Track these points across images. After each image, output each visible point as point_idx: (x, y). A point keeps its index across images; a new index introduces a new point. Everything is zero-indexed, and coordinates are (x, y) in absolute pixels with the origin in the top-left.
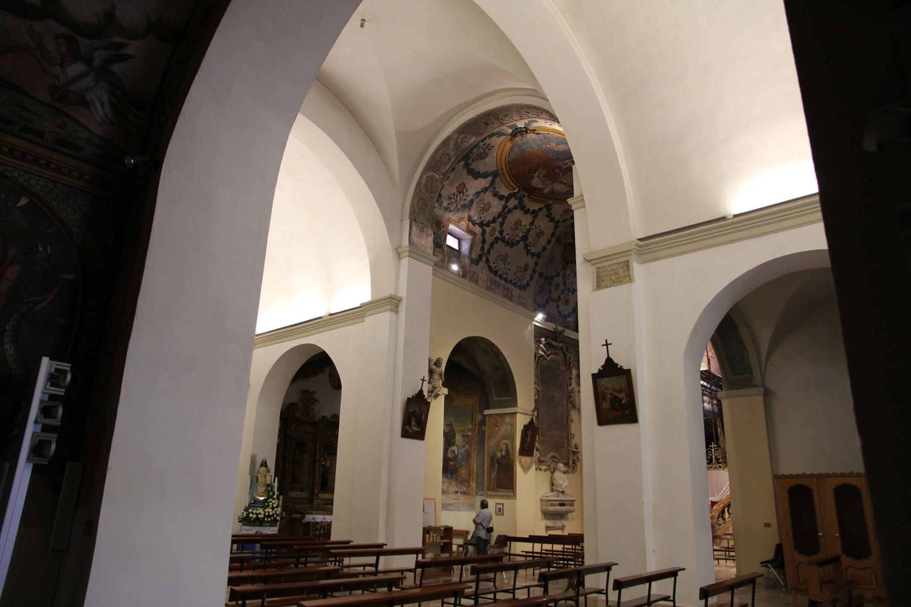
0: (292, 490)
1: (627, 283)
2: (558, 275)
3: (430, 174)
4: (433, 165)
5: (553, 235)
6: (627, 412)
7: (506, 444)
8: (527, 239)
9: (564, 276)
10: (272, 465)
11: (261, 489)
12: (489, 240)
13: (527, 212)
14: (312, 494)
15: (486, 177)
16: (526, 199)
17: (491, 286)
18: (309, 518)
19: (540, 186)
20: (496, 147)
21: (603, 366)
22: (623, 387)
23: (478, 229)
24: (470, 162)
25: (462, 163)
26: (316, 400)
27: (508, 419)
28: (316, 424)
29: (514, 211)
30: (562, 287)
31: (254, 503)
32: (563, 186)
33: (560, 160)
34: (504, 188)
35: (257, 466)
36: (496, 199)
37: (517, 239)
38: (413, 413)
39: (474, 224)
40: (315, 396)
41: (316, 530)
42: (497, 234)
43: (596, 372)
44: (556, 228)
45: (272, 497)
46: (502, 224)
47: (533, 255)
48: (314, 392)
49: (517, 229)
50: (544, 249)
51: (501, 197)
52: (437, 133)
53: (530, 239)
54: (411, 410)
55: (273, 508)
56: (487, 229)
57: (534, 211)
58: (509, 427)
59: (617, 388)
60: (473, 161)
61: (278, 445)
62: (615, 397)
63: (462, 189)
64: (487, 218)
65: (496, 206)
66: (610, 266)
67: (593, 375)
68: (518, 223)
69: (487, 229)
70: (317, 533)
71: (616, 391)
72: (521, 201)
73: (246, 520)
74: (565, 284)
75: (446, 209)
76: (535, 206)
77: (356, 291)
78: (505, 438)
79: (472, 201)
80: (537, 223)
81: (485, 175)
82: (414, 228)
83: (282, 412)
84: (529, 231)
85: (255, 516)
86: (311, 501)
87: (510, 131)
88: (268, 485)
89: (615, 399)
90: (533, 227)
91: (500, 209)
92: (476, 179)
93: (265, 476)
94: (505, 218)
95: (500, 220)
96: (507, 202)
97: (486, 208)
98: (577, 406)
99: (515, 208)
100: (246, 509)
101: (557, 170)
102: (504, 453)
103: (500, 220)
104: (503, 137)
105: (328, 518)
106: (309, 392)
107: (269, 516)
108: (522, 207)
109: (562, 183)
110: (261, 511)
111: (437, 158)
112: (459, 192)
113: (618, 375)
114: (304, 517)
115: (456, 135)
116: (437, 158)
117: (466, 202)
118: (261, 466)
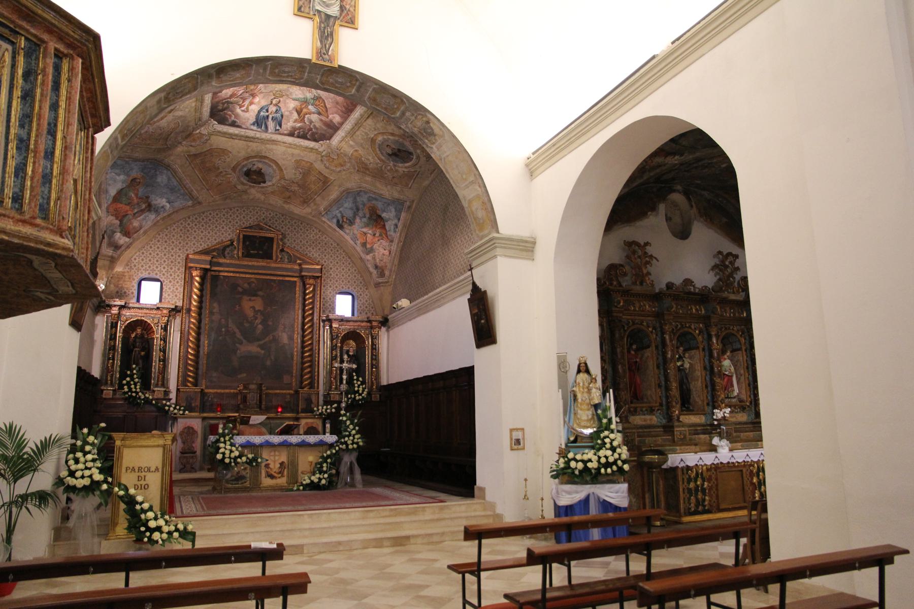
0: (634, 412)
10: (596, 368)
11: (585, 414)
14: (670, 418)
18: (675, 459)
26: (651, 256)
28: (657, 297)
31: (575, 441)
35: (569, 372)
40: (650, 250)
41: (689, 480)
45: (607, 428)
48: (647, 244)
55: (613, 449)
61: (602, 338)
70: (692, 485)
73: (565, 474)
83: (598, 280)
85: (580, 466)
86: (668, 428)
88: (596, 407)
93: (589, 391)
100: (563, 454)
105: (754, 455)
106: (638, 244)
107: (608, 465)
110: (590, 454)
114: (666, 461)
118: (579, 371)
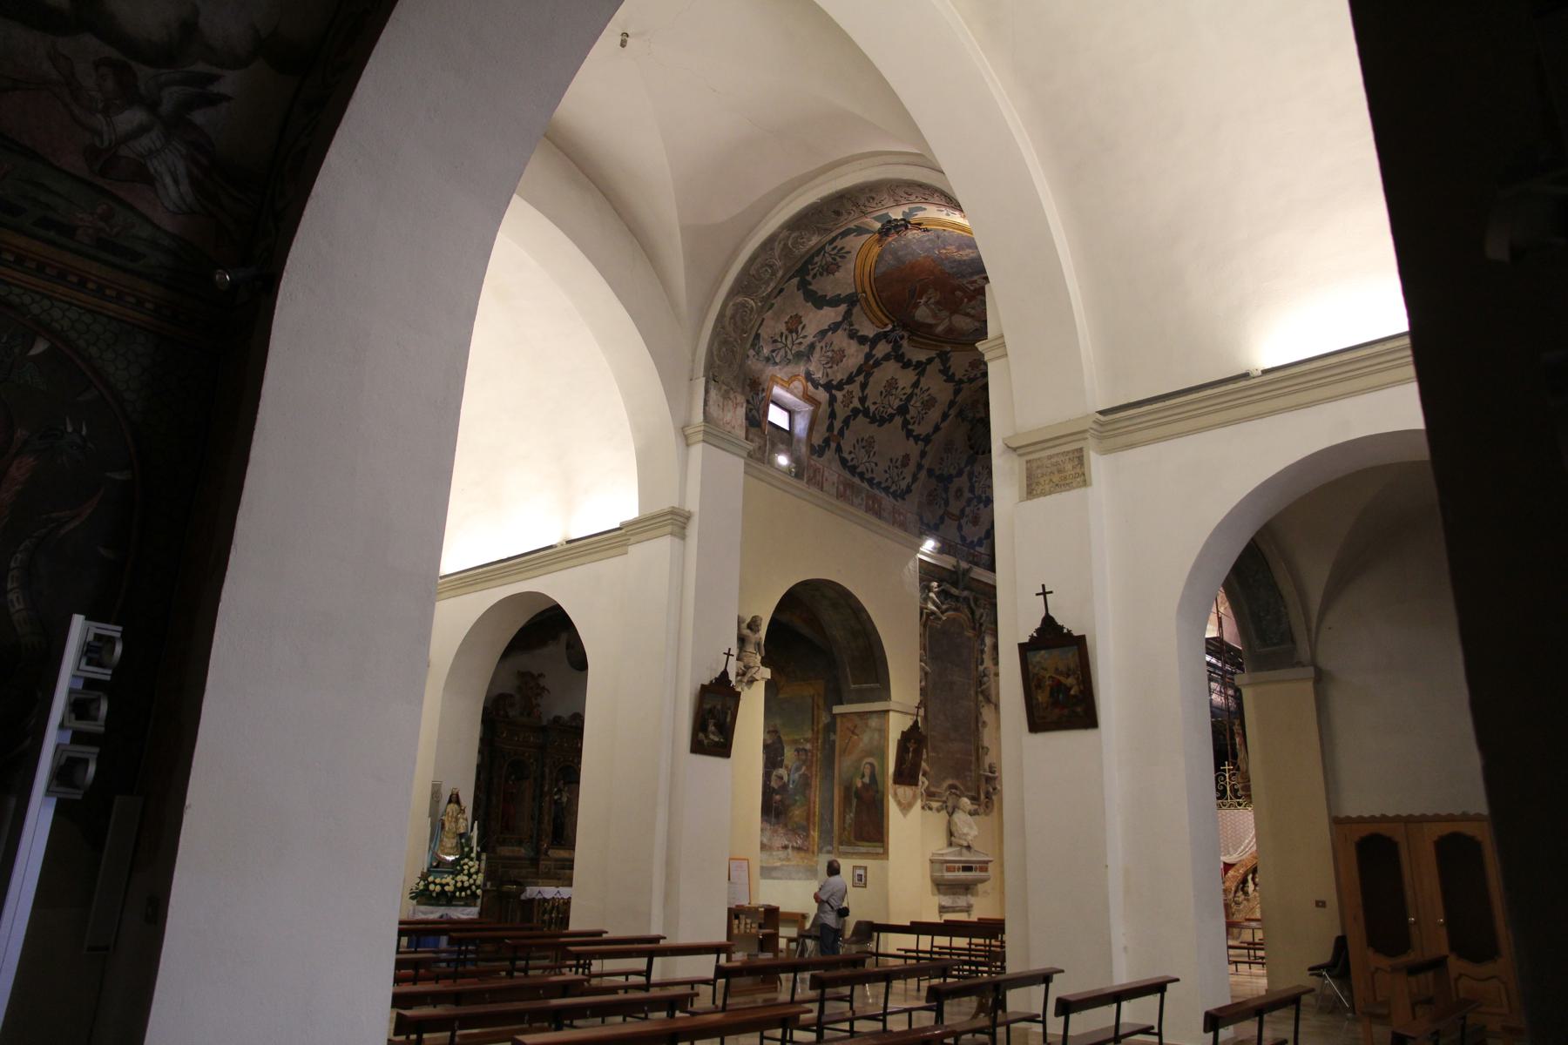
0: (503, 843)
1: (1079, 487)
2: (960, 473)
3: (740, 299)
4: (744, 285)
5: (952, 404)
6: (1079, 709)
7: (872, 765)
8: (907, 411)
9: (971, 475)
10: (467, 800)
11: (450, 842)
12: (842, 413)
13: (906, 365)
14: (538, 851)
15: (837, 305)
16: (905, 343)
17: (845, 493)
18: (531, 892)
19: (930, 321)
20: (854, 254)
21: (1037, 631)
22: (1072, 666)
23: (822, 395)
24: (809, 278)
25: (795, 281)
26: (543, 688)
27: (874, 722)
28: (543, 729)
29: (885, 364)
30: (967, 495)
31: (438, 866)
32: (968, 320)
33: (963, 276)
34: (867, 323)
35: (442, 802)
36: (854, 343)
37: (890, 411)
38: (711, 711)
39: (816, 385)
40: (542, 682)
41: (544, 912)
42: (856, 403)
43: (1026, 640)
44: (957, 392)
45: (468, 856)
46: (864, 386)
47: (917, 438)
48: (541, 675)
49: (889, 394)
50: (937, 428)
51: (862, 340)
52: (752, 229)
53: (912, 412)
54: (707, 706)
55: (470, 875)
56: (839, 395)
57: (919, 364)
58: (876, 736)
59: (1062, 667)
60: (814, 276)
61: (479, 767)
62: (1059, 683)
63: (794, 325)
64: (839, 375)
65: (854, 355)
66: (1050, 457)
67: (1021, 646)
68: (892, 384)
69: (839, 395)
70: (546, 917)
71: (1061, 673)
72: (897, 346)
73: (423, 896)
74: (972, 490)
75: (768, 359)
76: (920, 356)
77: (613, 501)
78: (869, 753)
79: (812, 347)
80: (924, 383)
81: (834, 302)
82: (713, 393)
83: (485, 709)
84: (910, 397)
85: (438, 888)
86: (535, 862)
87: (878, 225)
88: (461, 836)
89: (1058, 688)
90: (917, 391)
91: (860, 359)
92: (820, 308)
93: (457, 820)
94: (868, 375)
95: (861, 378)
96: (872, 348)
97: (837, 357)
98: (993, 699)
99: (887, 358)
100: (424, 877)
101: (958, 293)
102: (867, 780)
103: (861, 378)
104: (867, 236)
105: (565, 892)
106: (532, 675)
107: (463, 889)
108: (899, 357)
109: (968, 315)
110: (448, 879)
111: (752, 272)
112: (791, 331)
113: (1063, 646)
114: (523, 891)
115: (785, 233)
116: (752, 272)
117: (802, 348)
118: (450, 802)
